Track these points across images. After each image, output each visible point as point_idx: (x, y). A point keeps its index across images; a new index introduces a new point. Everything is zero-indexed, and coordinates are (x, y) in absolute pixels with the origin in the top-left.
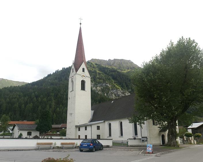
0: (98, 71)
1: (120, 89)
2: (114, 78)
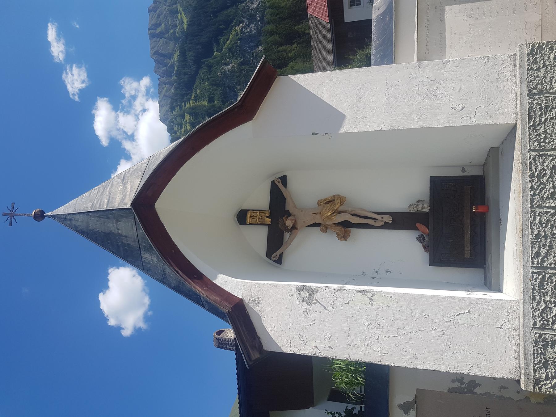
0: (191, 103)
1: (238, 28)
2: (207, 51)
